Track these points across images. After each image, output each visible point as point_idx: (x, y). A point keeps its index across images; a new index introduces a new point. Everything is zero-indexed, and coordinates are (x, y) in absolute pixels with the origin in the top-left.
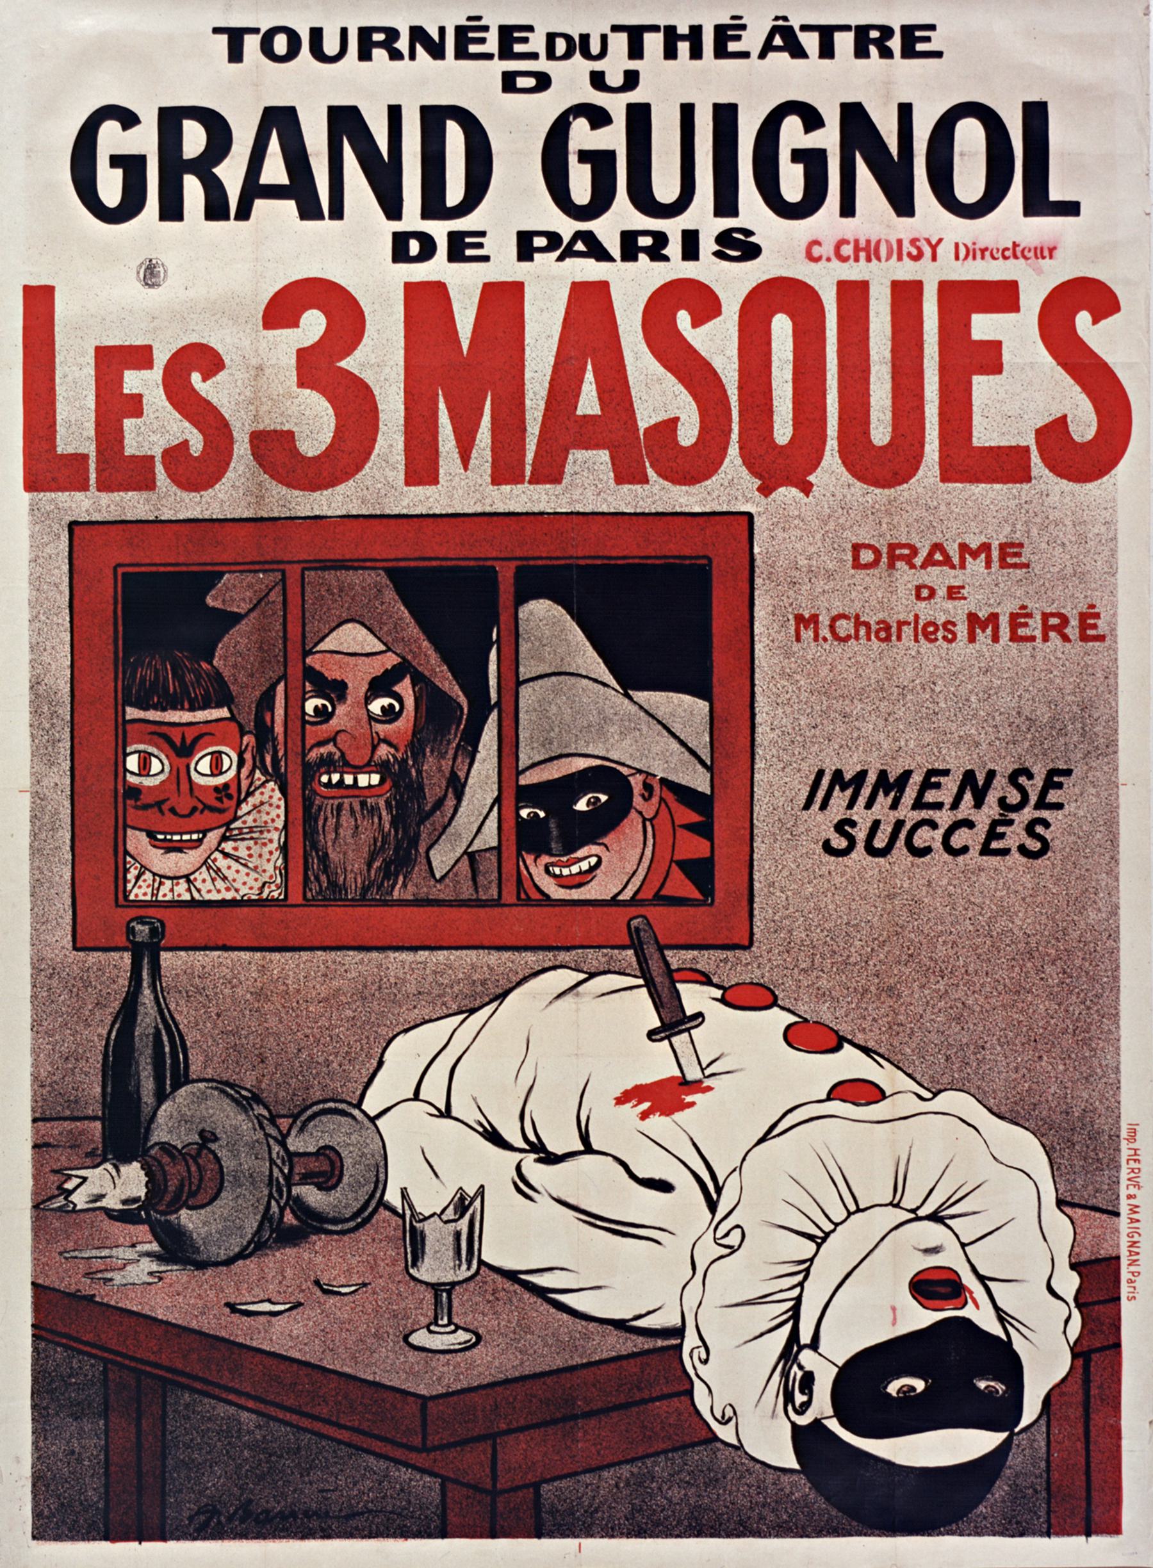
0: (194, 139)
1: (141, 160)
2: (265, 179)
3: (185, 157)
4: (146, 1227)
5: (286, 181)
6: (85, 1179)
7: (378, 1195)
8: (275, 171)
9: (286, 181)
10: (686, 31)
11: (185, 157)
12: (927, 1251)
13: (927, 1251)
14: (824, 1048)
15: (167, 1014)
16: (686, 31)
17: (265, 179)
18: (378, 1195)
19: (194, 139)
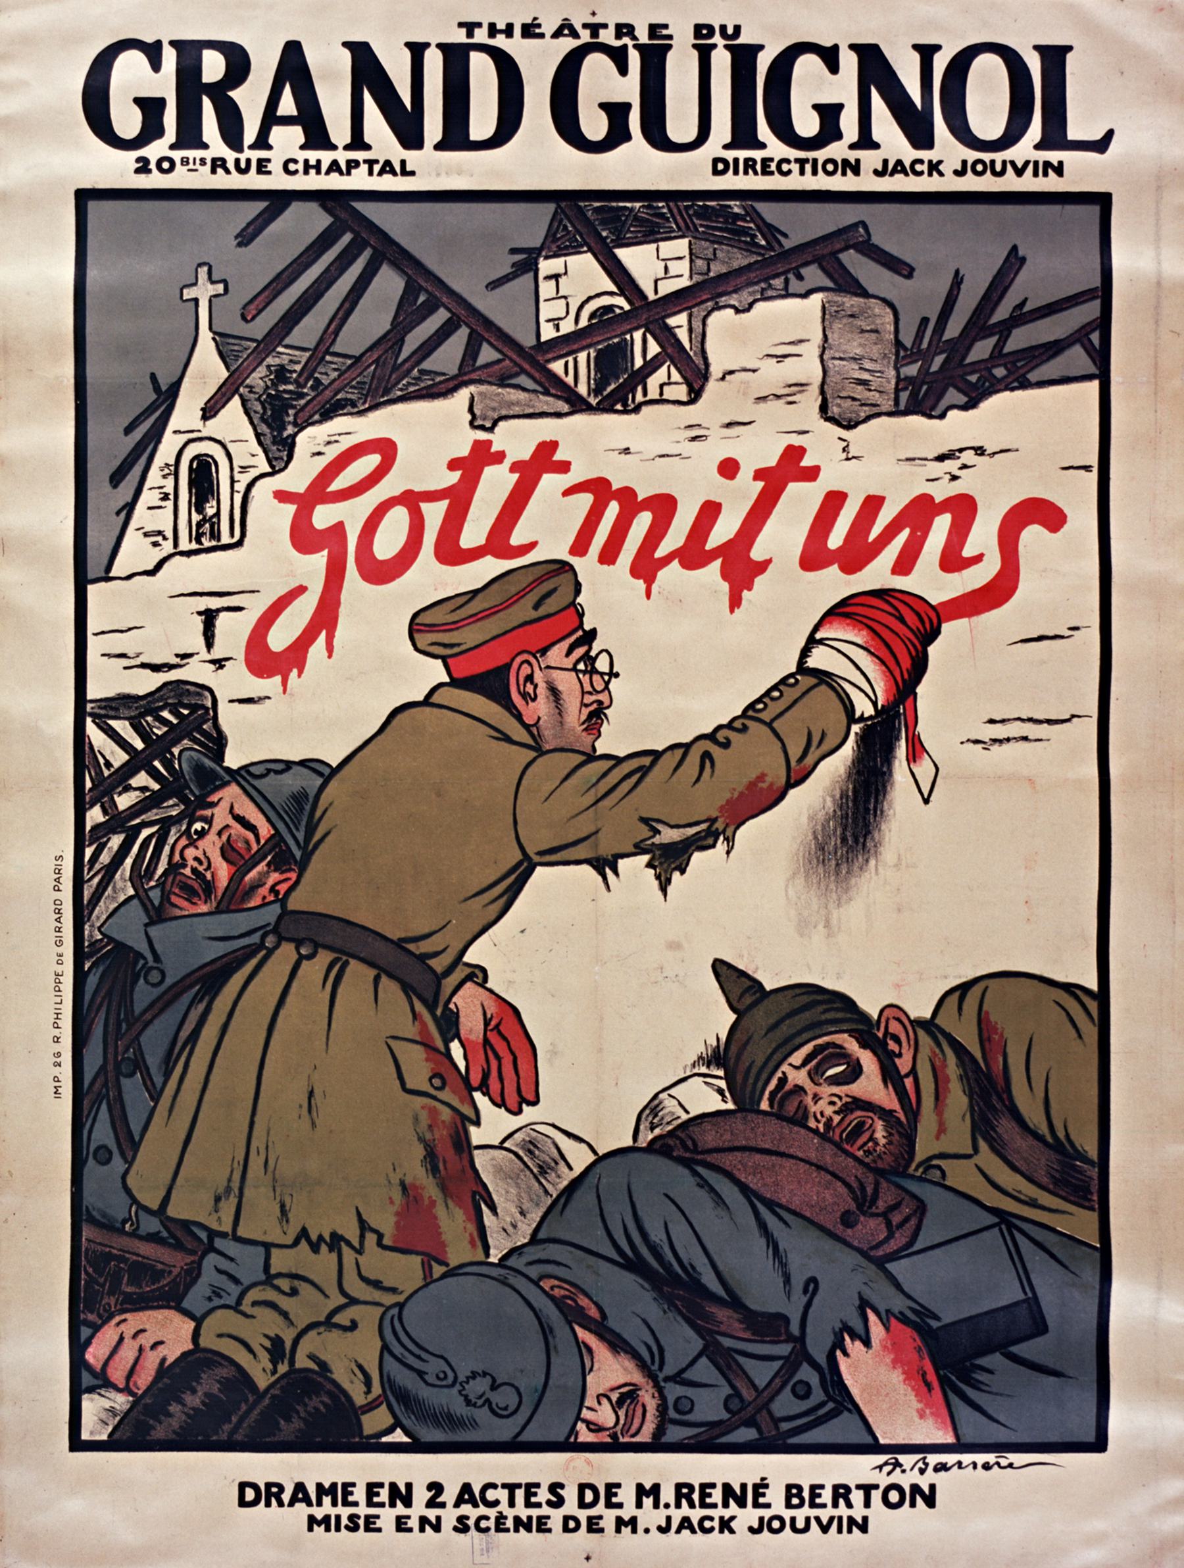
0: (213, 67)
1: (161, 103)
2: (281, 112)
3: (204, 80)
4: (226, 374)
5: (295, 113)
6: (387, 449)
7: (150, 907)
8: (287, 105)
9: (295, 113)
10: (503, 27)
11: (204, 80)
12: (794, 402)
13: (794, 402)
14: (515, 573)
15: (333, 327)
16: (503, 27)
17: (281, 112)
18: (150, 907)
19: (213, 67)
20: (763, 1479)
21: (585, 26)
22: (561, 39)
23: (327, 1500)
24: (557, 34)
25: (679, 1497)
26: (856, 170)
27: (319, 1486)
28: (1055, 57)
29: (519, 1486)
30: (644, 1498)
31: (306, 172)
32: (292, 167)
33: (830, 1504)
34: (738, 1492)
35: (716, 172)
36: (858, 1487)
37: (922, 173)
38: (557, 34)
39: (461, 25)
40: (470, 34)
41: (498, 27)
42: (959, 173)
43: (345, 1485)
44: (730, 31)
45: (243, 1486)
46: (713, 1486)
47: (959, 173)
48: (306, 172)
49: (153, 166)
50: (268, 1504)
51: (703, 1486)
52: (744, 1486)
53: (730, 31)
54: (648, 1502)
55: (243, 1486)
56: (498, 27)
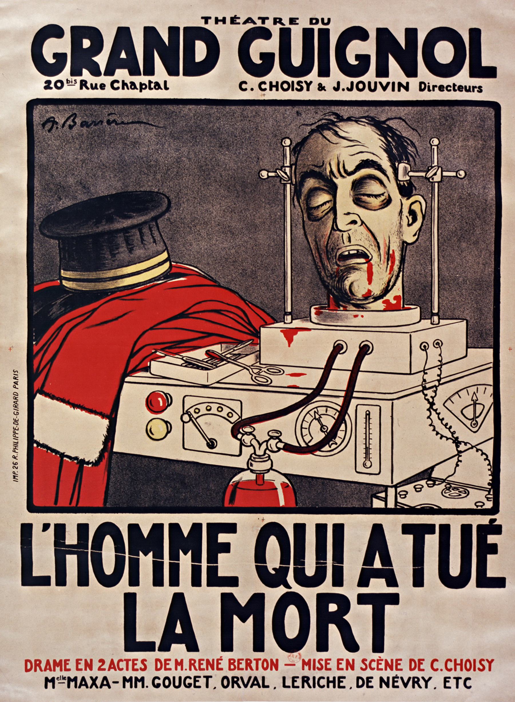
20: (221, 657)
21: (259, 18)
22: (247, 24)
23: (306, 668)
24: (245, 23)
25: (191, 664)
26: (407, 88)
27: (55, 661)
28: (475, 34)
29: (130, 660)
30: (305, 666)
31: (271, 89)
32: (263, 86)
33: (345, 668)
34: (211, 662)
35: (421, 90)
36: (254, 660)
37: (118, 88)
38: (245, 23)
39: (202, 18)
40: (263, 23)
41: (219, 19)
42: (350, 89)
43: (66, 661)
44: (326, 21)
45: (27, 661)
46: (342, 660)
47: (336, 89)
48: (271, 89)
49: (98, 87)
50: (271, 669)
51: (239, 660)
52: (213, 660)
53: (326, 21)
54: (179, 668)
55: (27, 661)
56: (219, 19)
